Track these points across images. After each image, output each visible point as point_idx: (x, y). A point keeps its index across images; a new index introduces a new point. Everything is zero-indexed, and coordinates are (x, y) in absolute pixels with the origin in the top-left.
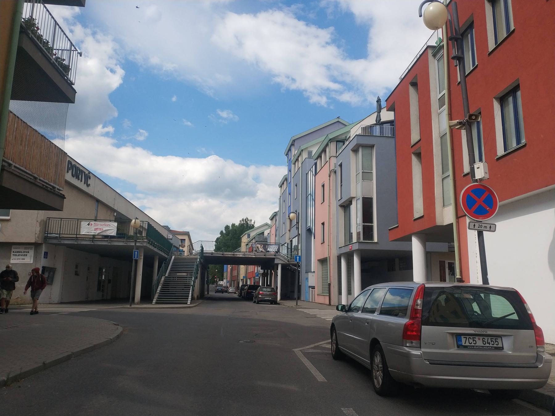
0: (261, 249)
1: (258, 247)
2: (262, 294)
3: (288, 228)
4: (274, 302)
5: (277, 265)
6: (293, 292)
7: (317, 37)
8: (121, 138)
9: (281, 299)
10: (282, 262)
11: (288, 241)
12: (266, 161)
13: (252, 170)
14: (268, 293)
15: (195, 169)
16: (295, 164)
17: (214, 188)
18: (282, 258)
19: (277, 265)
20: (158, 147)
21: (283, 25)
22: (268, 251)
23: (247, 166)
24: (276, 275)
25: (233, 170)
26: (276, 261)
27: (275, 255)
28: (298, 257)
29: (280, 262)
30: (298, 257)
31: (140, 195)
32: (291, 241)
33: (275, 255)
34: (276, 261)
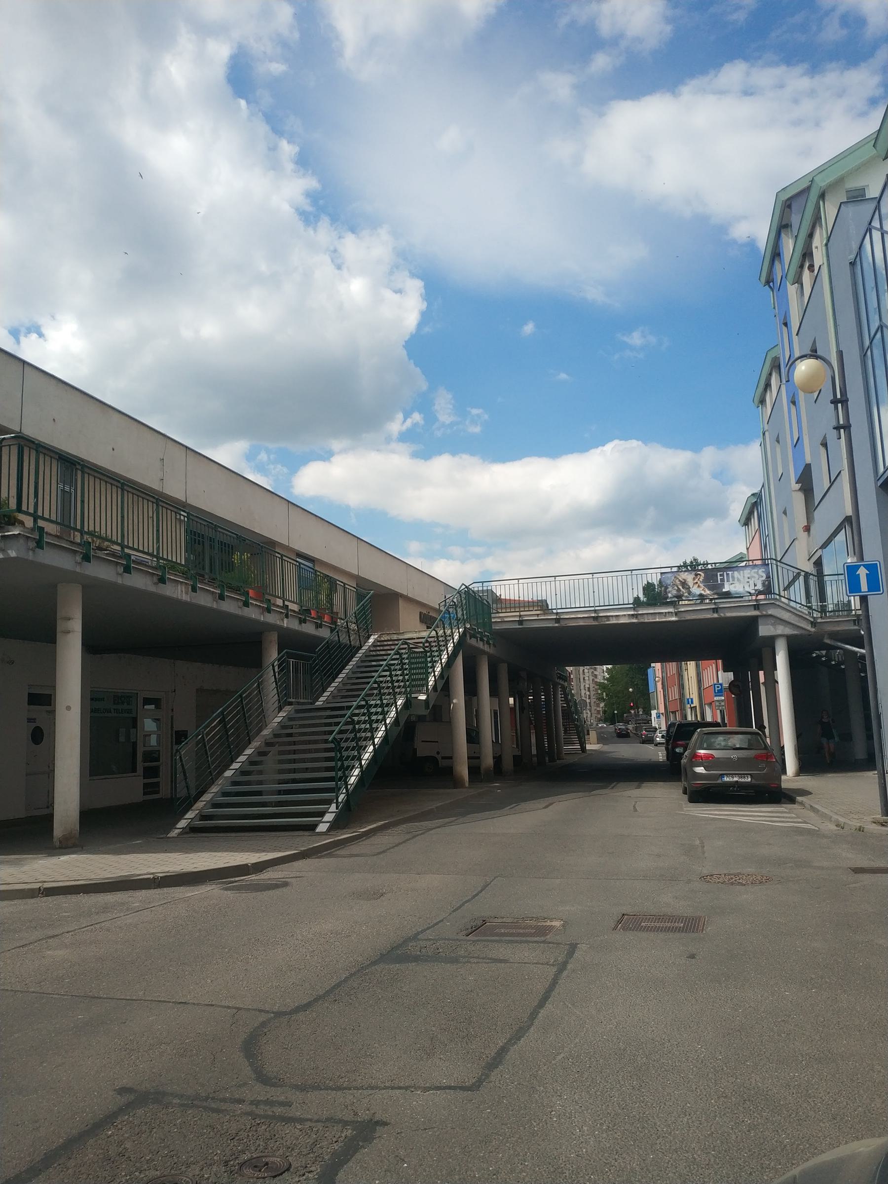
0: (696, 591)
1: (684, 584)
2: (708, 762)
3: (801, 519)
4: (769, 793)
5: (770, 642)
6: (847, 737)
7: (841, 93)
8: (426, 443)
9: (804, 768)
10: (788, 631)
11: (809, 567)
12: (745, 441)
13: (709, 456)
14: (734, 755)
15: (581, 477)
16: (798, 280)
17: (625, 512)
18: (786, 616)
19: (770, 642)
20: (499, 447)
21: (748, 92)
22: (728, 595)
23: (697, 450)
24: (772, 683)
25: (666, 463)
26: (764, 630)
27: (757, 607)
28: (862, 572)
29: (780, 630)
30: (862, 572)
31: (478, 550)
32: (818, 564)
33: (757, 607)
34: (764, 630)
